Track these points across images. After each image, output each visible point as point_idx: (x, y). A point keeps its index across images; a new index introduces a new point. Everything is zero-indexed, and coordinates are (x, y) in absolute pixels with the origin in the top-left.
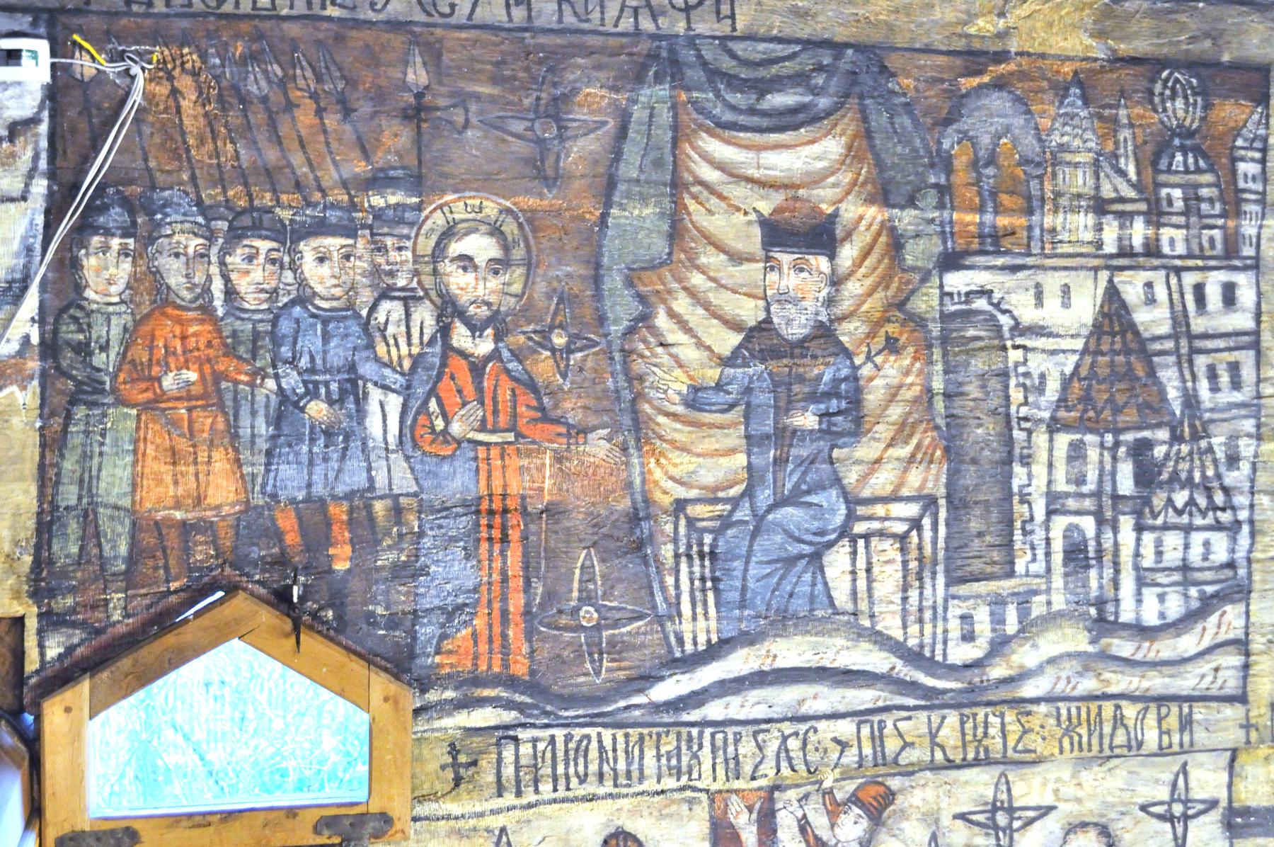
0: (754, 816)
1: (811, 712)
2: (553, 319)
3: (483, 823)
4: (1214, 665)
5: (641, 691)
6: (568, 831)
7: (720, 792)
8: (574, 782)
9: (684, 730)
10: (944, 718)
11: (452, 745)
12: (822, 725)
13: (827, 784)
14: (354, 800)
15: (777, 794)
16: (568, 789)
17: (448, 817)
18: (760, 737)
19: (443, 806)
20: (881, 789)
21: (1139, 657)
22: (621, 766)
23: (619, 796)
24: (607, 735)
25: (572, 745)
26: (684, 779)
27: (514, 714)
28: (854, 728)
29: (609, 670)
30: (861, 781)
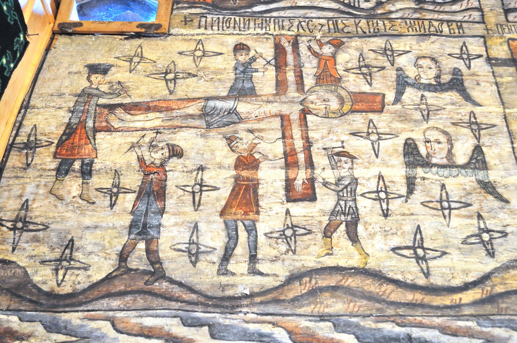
0: (291, 44)
1: (310, 16)
2: (347, 190)
3: (194, 38)
4: (469, 14)
5: (250, 8)
6: (223, 42)
7: (277, 35)
8: (225, 28)
9: (264, 19)
10: (360, 21)
11: (185, 16)
12: (314, 20)
13: (318, 37)
14: (254, 324)
15: (298, 38)
16: (223, 30)
17: (182, 35)
18: (291, 21)
19: (180, 30)
20: (339, 41)
21: (436, 9)
22: (242, 25)
23: (241, 34)
24: (237, 19)
25: (225, 20)
26: (264, 30)
27: (206, 11)
28: (326, 21)
29: (238, 3)
30: (331, 38)
